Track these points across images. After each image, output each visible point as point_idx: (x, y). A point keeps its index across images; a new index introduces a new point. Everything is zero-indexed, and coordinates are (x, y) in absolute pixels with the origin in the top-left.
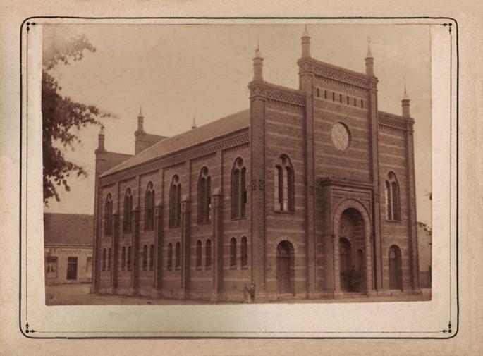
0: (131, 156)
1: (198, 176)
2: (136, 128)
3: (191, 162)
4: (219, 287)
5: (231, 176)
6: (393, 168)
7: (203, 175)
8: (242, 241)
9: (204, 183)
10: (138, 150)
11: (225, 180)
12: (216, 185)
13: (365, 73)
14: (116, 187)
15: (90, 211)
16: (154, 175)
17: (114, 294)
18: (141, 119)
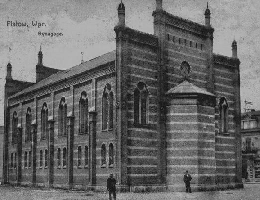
0: (34, 84)
1: (103, 92)
2: (36, 63)
3: (23, 105)
4: (33, 179)
5: (79, 105)
6: (225, 95)
7: (107, 91)
8: (110, 147)
9: (84, 103)
10: (39, 80)
11: (98, 101)
12: (51, 115)
13: (204, 25)
14: (35, 103)
15: (4, 125)
16: (48, 98)
17: (19, 184)
18: (40, 55)
